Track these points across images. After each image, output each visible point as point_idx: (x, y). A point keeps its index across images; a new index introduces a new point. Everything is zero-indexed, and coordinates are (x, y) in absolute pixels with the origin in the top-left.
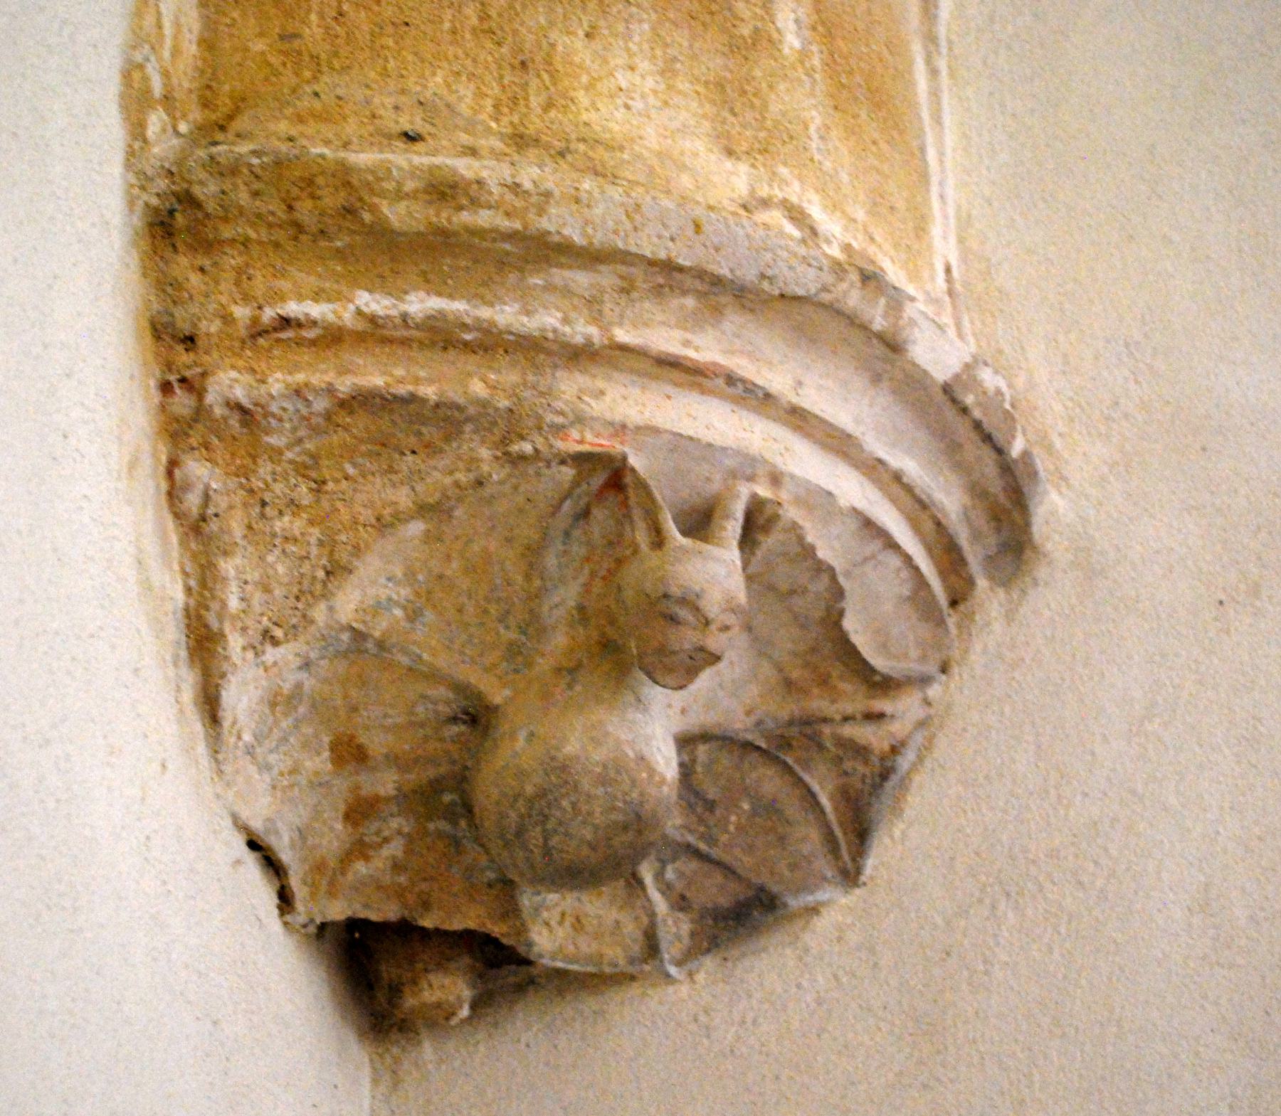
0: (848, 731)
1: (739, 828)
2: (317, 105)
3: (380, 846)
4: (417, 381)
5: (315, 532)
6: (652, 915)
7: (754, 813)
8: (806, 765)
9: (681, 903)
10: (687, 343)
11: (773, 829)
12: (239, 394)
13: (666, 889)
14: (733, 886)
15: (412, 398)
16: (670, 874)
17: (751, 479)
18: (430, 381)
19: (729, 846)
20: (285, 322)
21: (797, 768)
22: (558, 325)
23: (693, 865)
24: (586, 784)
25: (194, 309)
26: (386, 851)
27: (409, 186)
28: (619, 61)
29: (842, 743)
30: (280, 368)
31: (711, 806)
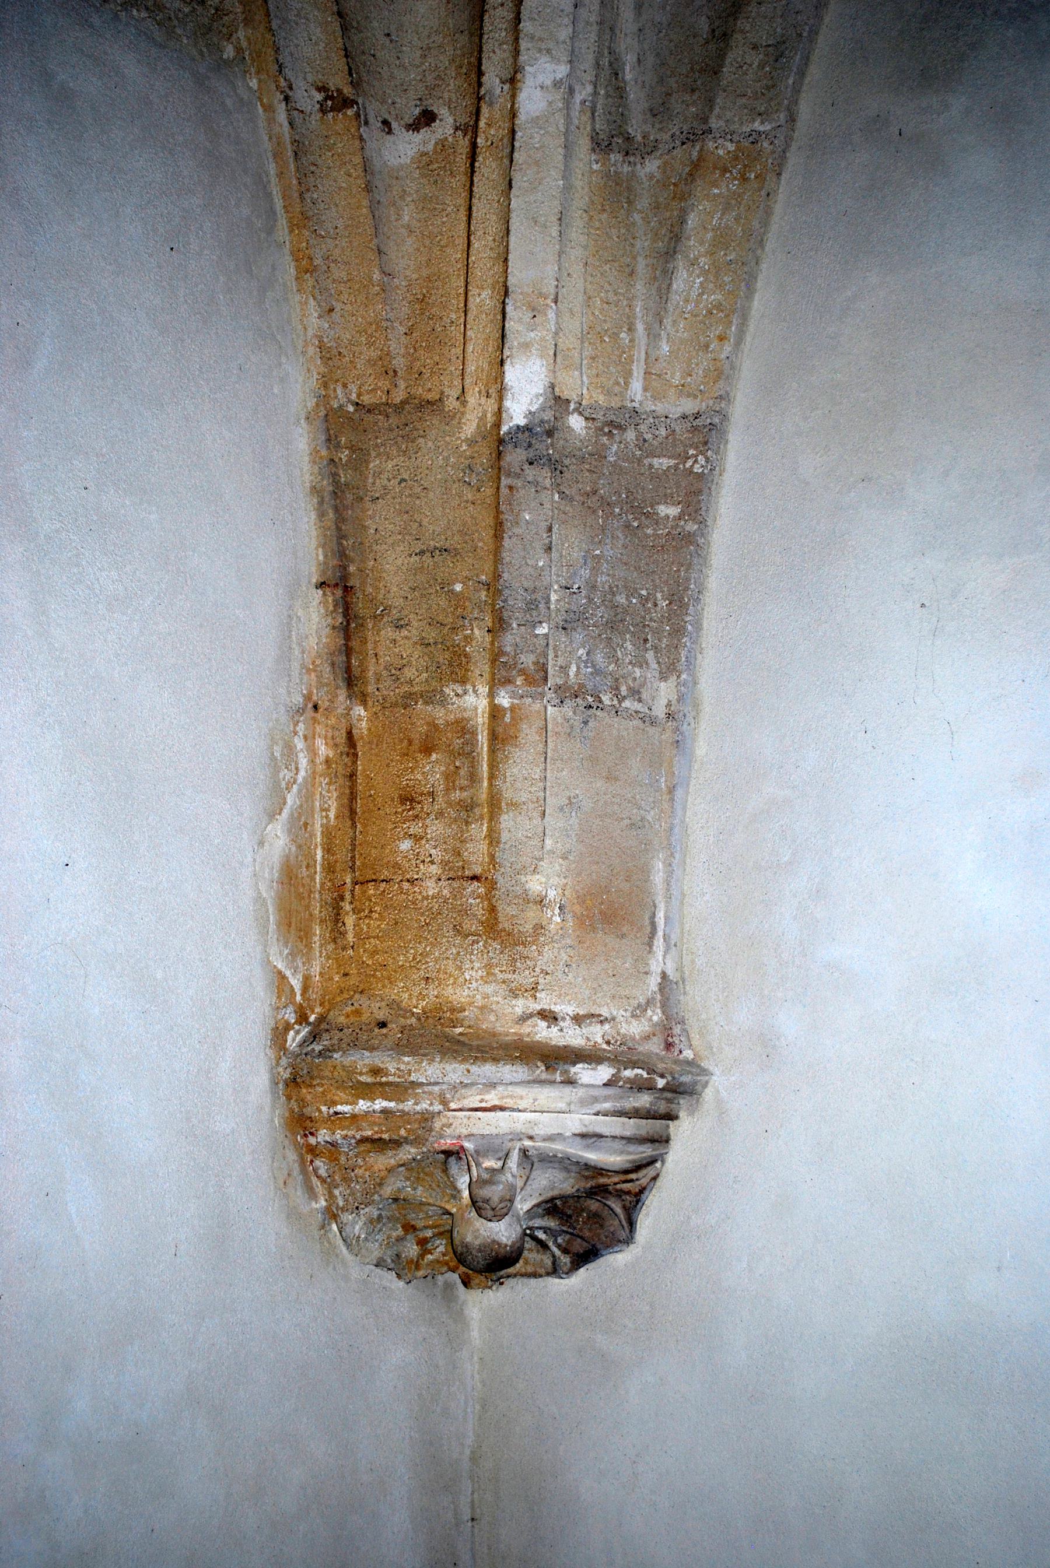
0: (618, 1186)
1: (584, 1222)
2: (353, 1008)
3: (435, 1249)
4: (382, 1132)
5: (368, 1173)
6: (554, 1256)
7: (589, 1218)
8: (607, 1199)
9: (565, 1251)
10: (481, 1101)
11: (597, 1223)
12: (328, 1139)
13: (559, 1246)
14: (585, 1244)
15: (380, 1139)
16: (560, 1240)
17: (520, 1140)
18: (387, 1132)
19: (581, 1230)
20: (336, 1113)
21: (604, 1201)
22: (428, 1107)
23: (568, 1237)
24: (474, 1252)
25: (309, 1109)
26: (438, 1250)
27: (364, 1070)
28: (467, 966)
29: (617, 1190)
30: (339, 1128)
31: (570, 1217)
